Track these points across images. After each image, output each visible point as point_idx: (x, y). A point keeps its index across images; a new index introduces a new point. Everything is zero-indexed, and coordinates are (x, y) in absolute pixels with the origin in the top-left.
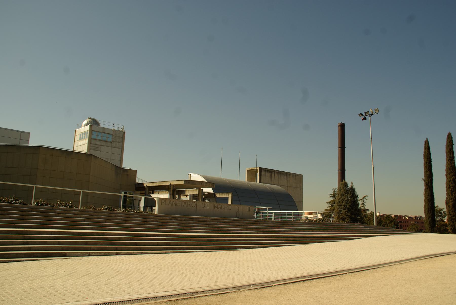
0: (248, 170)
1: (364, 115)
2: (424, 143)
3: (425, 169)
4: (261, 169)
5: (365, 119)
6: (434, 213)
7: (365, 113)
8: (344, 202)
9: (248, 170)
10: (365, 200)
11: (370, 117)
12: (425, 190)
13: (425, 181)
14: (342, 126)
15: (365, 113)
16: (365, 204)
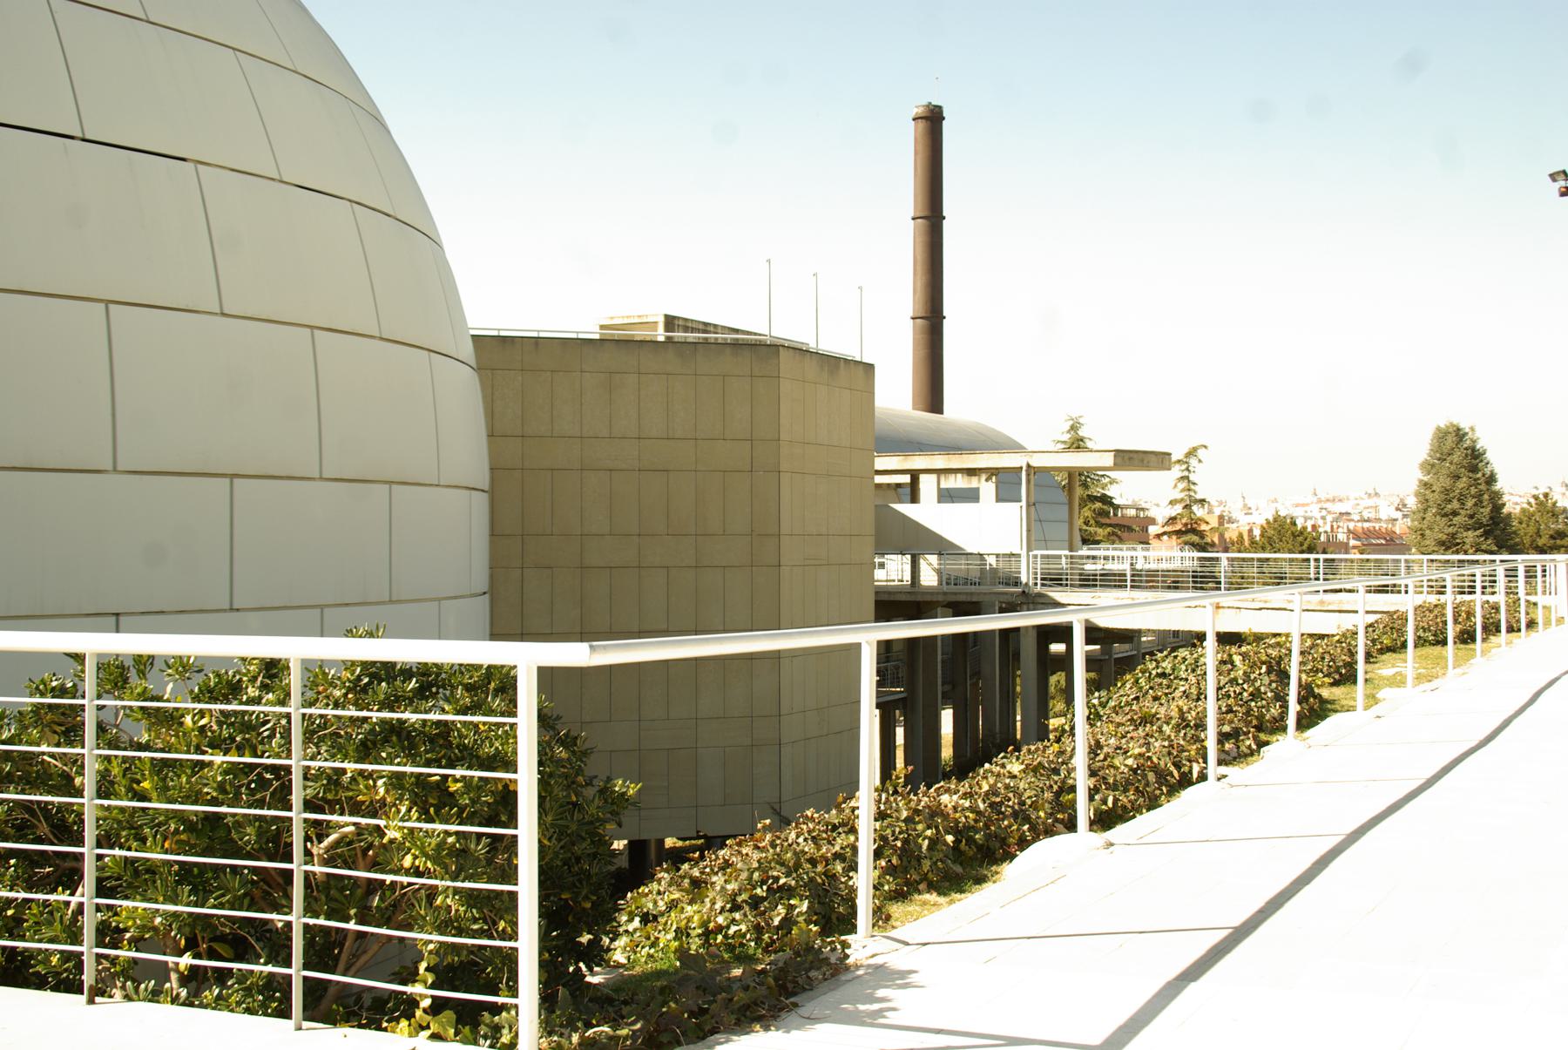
8: (1470, 503)
10: (1193, 462)
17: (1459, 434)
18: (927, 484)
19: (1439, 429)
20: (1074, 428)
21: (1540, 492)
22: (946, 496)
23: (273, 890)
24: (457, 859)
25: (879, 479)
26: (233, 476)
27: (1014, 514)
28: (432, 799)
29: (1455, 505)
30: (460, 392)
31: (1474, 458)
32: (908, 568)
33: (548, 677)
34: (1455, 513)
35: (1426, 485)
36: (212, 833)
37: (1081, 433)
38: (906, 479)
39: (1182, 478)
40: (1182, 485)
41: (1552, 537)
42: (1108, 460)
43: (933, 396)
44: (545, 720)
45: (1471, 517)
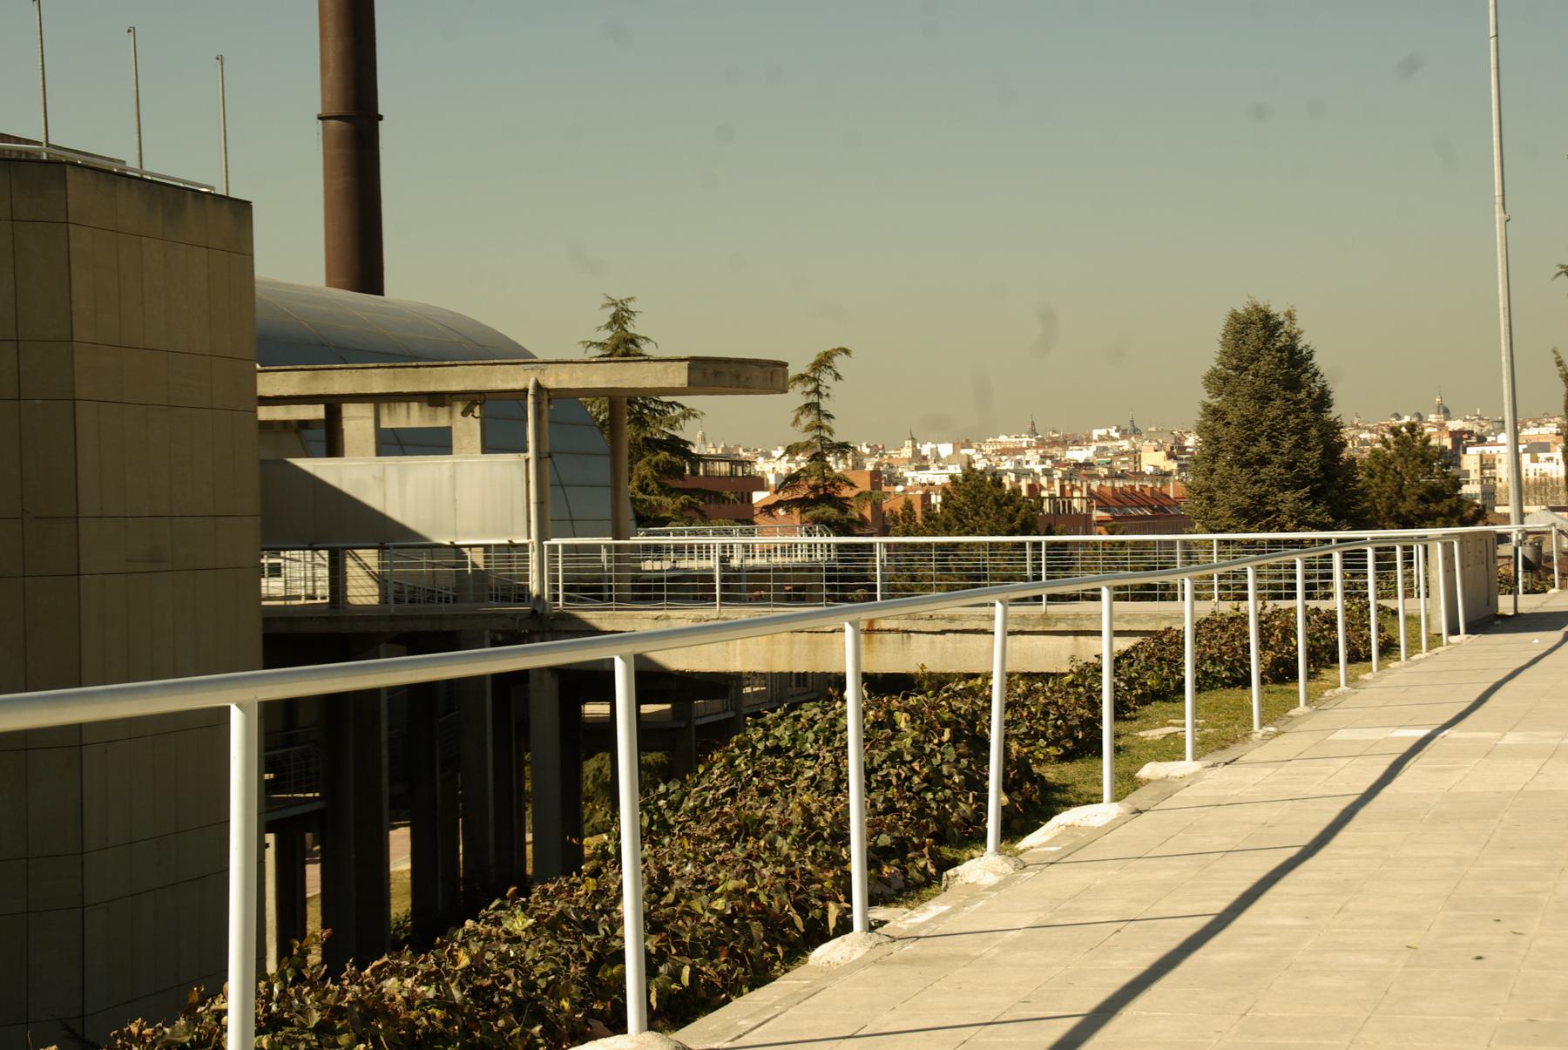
10: (826, 378)
16: (825, 405)
18: (358, 424)
19: (1234, 316)
29: (1264, 446)
34: (1263, 461)
38: (317, 412)
40: (806, 420)
41: (1422, 499)
42: (678, 376)
45: (1290, 466)
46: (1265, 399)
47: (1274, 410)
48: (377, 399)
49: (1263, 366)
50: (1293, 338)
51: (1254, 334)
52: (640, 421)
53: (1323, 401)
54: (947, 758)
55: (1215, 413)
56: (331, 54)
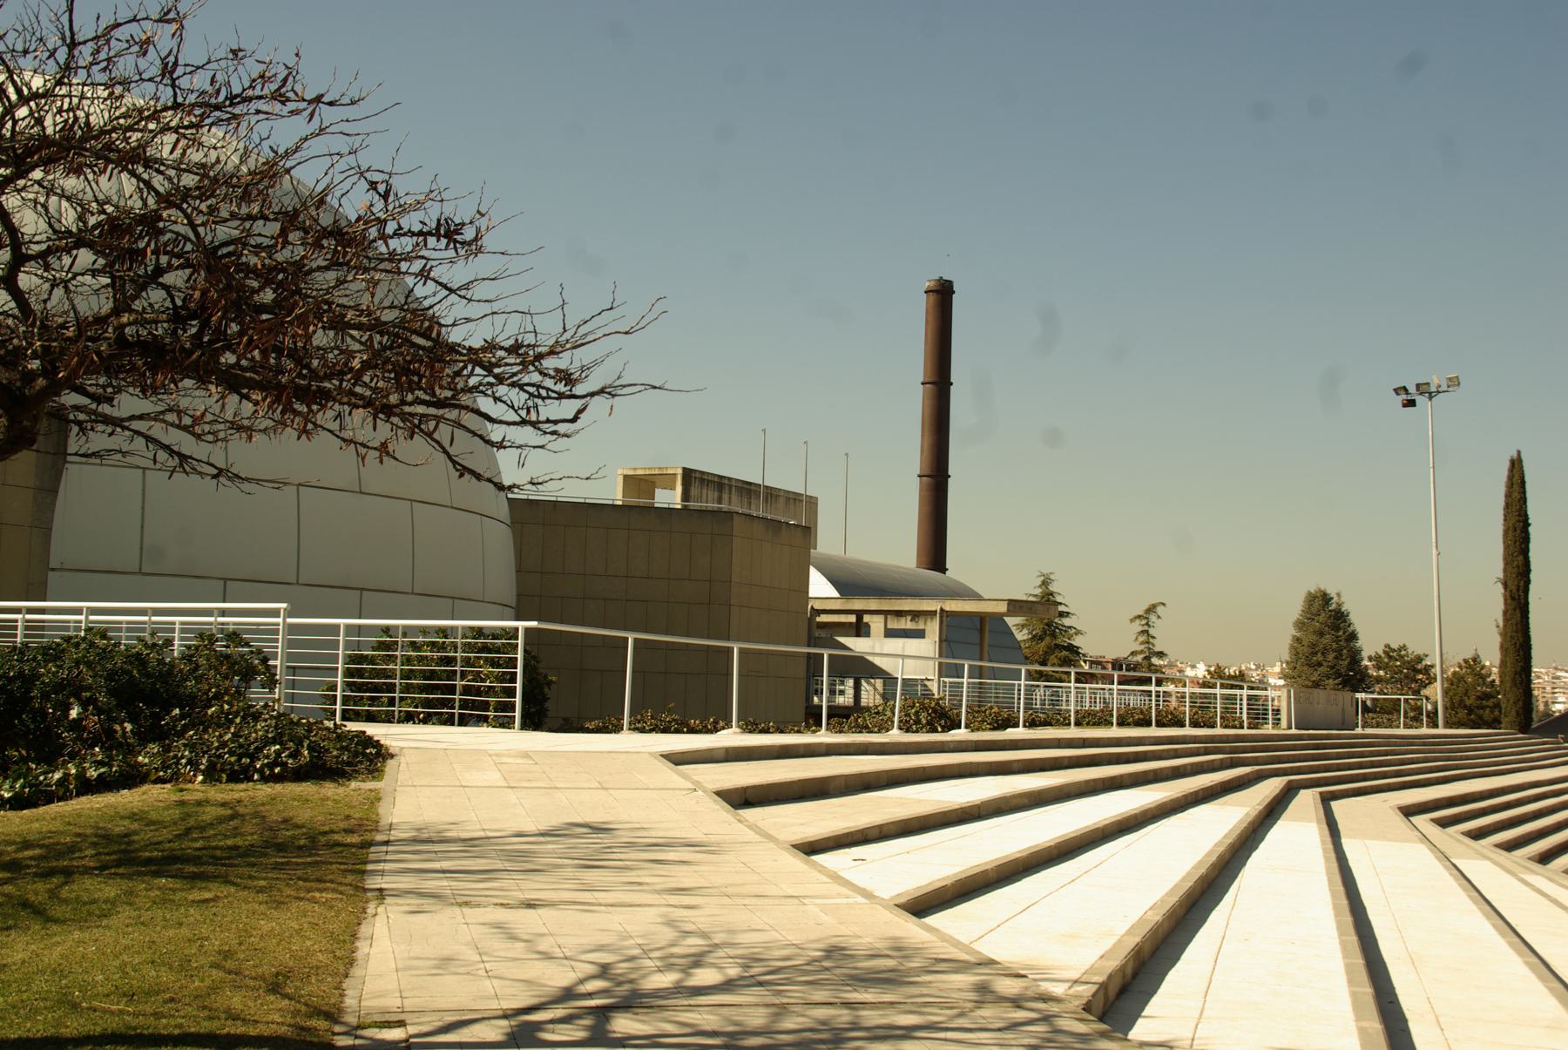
0: (626, 477)
1: (1412, 389)
2: (1507, 465)
3: (1506, 547)
4: (688, 473)
5: (1411, 403)
6: (1529, 681)
7: (1418, 386)
8: (1331, 656)
9: (626, 477)
10: (1153, 618)
11: (1430, 398)
12: (1505, 613)
13: (1505, 585)
14: (943, 294)
15: (1418, 386)
16: (1152, 631)
17: (1325, 598)
18: (876, 624)
19: (1310, 594)
20: (1045, 583)
21: (1469, 655)
22: (890, 633)
23: (451, 675)
24: (500, 678)
25: (823, 618)
26: (362, 589)
27: (927, 646)
28: (494, 663)
29: (1319, 657)
30: (499, 542)
31: (1339, 619)
32: (864, 694)
33: (527, 630)
34: (1320, 664)
35: (1298, 640)
36: (432, 675)
37: (1052, 588)
38: (852, 619)
39: (1143, 632)
40: (1141, 639)
41: (1479, 698)
42: (1003, 608)
43: (935, 552)
44: (525, 651)
45: (1332, 667)
46: (1321, 634)
47: (1327, 639)
48: (886, 613)
49: (1321, 619)
50: (1339, 605)
51: (1317, 604)
52: (1054, 636)
53: (1353, 637)
54: (889, 713)
55: (1298, 640)
56: (926, 445)
